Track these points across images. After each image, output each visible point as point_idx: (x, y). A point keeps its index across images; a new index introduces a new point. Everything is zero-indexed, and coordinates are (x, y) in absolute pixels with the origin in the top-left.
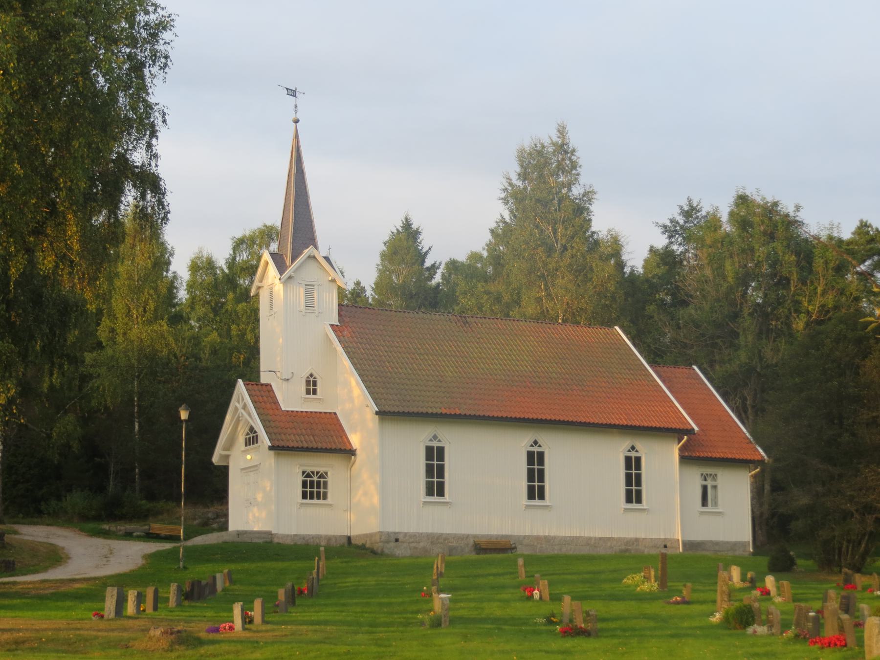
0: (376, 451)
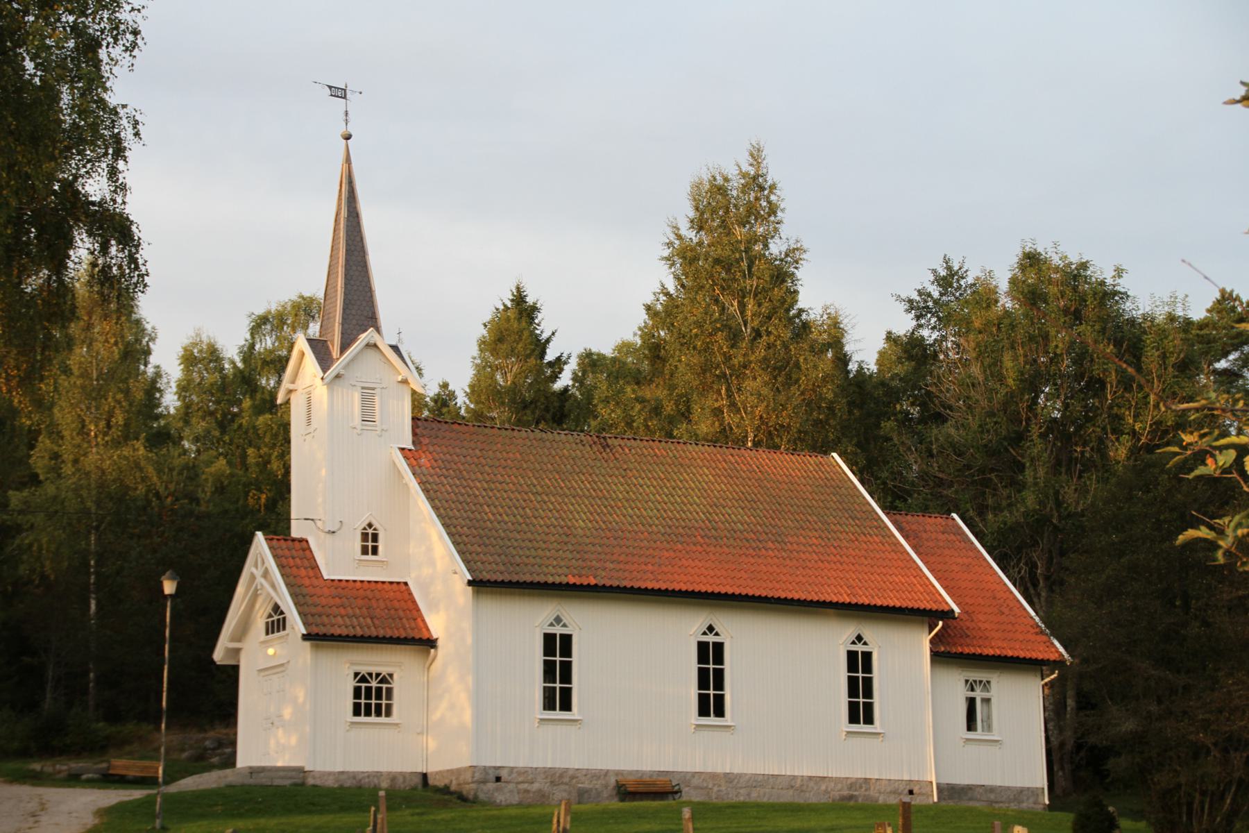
0: (469, 640)
